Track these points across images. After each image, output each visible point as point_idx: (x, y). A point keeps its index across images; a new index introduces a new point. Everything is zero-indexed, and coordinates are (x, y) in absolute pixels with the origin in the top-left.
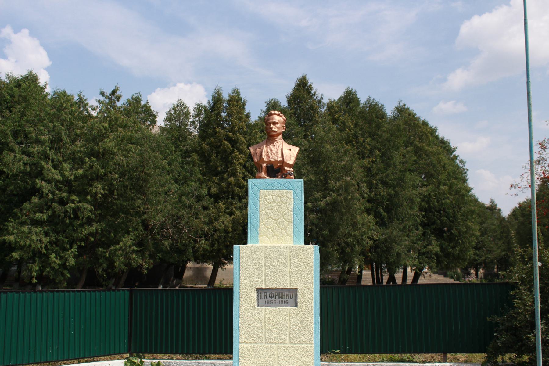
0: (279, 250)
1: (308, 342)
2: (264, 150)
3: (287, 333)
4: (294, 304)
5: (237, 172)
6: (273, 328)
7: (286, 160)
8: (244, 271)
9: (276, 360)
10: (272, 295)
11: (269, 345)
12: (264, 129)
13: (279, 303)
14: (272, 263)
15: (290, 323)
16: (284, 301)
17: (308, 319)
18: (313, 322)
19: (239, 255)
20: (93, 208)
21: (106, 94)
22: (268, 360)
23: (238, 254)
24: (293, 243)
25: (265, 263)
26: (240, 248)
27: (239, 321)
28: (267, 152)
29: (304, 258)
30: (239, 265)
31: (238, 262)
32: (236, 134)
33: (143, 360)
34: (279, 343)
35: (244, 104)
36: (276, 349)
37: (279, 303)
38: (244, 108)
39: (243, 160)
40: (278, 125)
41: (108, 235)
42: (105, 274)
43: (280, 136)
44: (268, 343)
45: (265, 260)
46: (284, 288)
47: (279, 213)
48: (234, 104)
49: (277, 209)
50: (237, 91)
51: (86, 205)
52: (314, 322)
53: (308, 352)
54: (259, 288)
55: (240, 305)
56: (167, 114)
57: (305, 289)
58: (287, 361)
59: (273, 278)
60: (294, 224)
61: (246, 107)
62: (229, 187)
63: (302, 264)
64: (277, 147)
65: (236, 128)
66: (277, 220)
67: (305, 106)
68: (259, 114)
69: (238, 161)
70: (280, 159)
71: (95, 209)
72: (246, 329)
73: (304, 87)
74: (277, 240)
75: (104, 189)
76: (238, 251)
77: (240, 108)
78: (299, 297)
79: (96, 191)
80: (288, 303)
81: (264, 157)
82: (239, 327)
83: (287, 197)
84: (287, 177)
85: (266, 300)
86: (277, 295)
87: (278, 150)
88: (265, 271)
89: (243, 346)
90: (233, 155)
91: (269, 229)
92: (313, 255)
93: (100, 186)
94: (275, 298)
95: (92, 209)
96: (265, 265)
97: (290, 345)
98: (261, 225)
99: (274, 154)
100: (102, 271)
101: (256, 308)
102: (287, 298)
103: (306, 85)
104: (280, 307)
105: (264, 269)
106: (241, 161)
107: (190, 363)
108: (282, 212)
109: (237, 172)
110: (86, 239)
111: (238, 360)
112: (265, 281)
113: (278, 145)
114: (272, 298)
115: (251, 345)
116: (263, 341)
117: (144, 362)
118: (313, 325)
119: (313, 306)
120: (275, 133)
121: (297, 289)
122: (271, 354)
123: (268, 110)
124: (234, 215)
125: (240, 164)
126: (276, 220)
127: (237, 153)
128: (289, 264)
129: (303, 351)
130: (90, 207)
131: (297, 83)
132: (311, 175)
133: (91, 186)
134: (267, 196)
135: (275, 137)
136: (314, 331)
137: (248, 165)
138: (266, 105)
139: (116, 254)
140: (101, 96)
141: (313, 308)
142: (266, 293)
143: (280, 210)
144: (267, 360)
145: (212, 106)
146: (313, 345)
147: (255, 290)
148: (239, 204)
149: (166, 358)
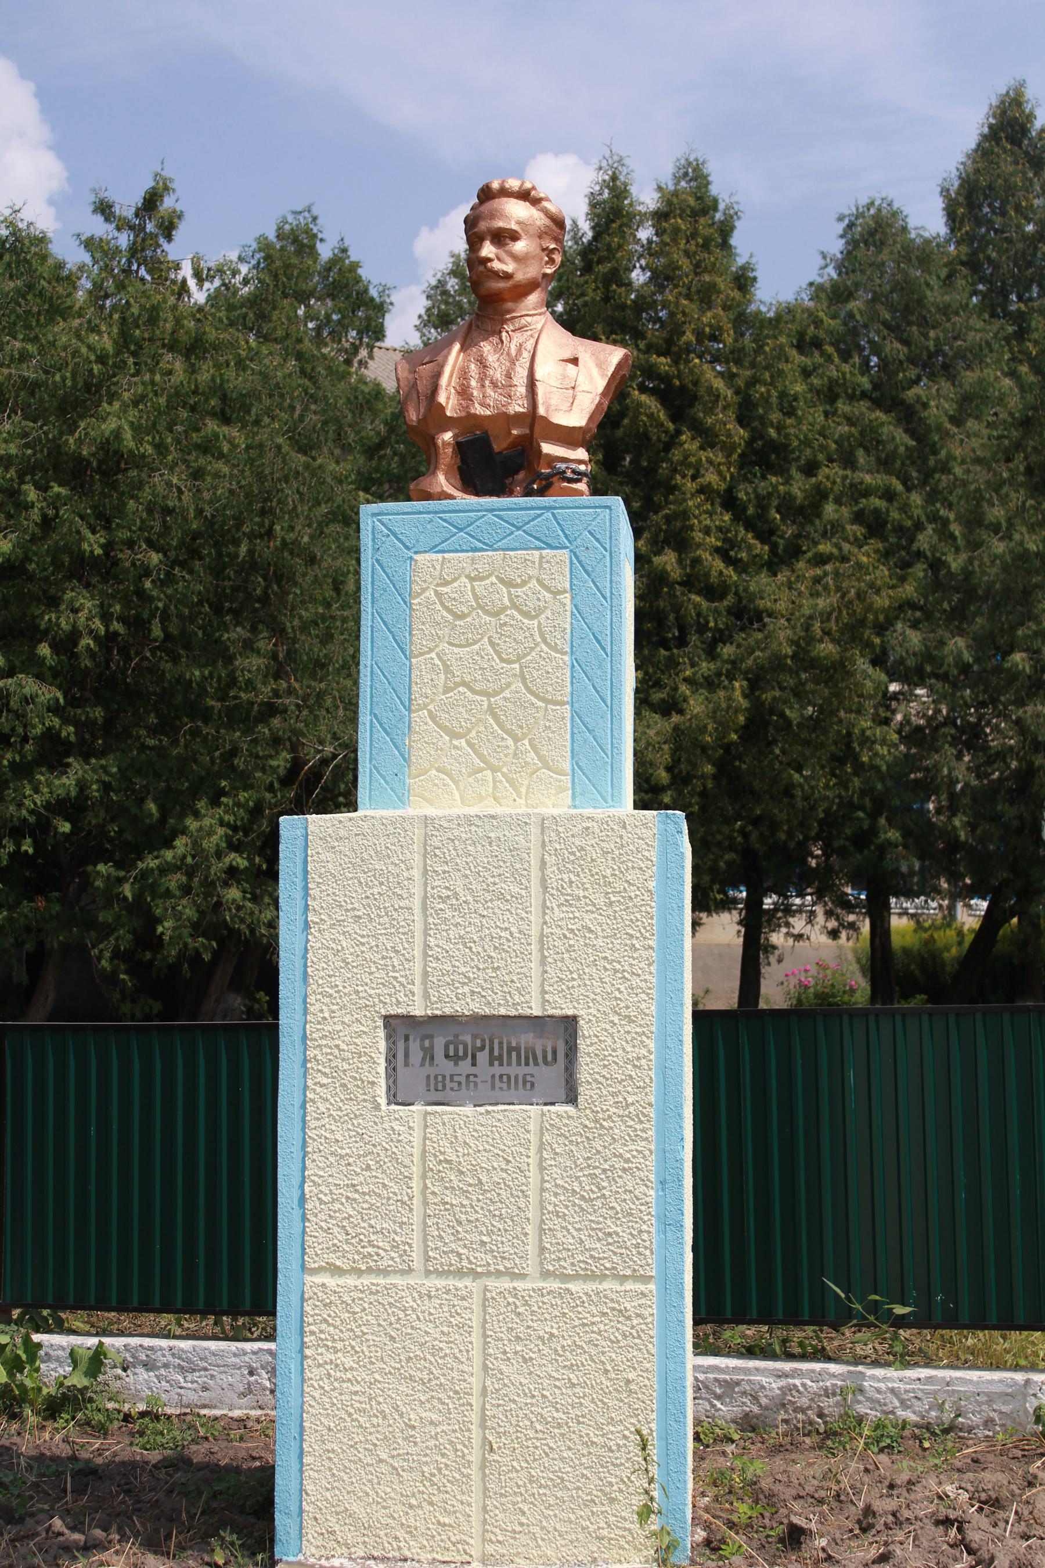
0: (492, 835)
1: (628, 1272)
2: (447, 370)
3: (529, 1229)
4: (562, 1094)
5: (691, 528)
6: (463, 1206)
7: (547, 411)
8: (327, 935)
9: (476, 1354)
10: (456, 1050)
11: (440, 1283)
12: (822, 334)
13: (493, 1087)
14: (456, 895)
15: (543, 1181)
16: (516, 1077)
17: (627, 1161)
18: (652, 1177)
19: (306, 862)
20: (59, 695)
21: (117, 210)
22: (435, 1351)
23: (299, 860)
24: (569, 802)
25: (425, 897)
26: (311, 828)
27: (304, 1168)
28: (464, 375)
29: (609, 872)
30: (307, 906)
31: (298, 895)
32: (688, 361)
33: (36, 1338)
34: (489, 1274)
35: (726, 230)
36: (476, 1301)
37: (493, 1087)
38: (725, 245)
39: (720, 473)
40: (520, 246)
41: (134, 810)
42: (127, 973)
43: (534, 298)
44: (436, 1271)
45: (426, 884)
46: (513, 1013)
47: (502, 660)
48: (676, 230)
49: (492, 644)
50: (697, 169)
51: (30, 685)
52: (657, 1174)
53: (629, 1318)
54: (397, 1016)
55: (310, 1095)
56: (428, 297)
57: (616, 1019)
58: (525, 1361)
59: (463, 969)
60: (575, 713)
61: (734, 241)
62: (658, 595)
63: (601, 901)
64: (513, 352)
65: (689, 336)
66: (496, 693)
67: (1019, 227)
68: (816, 271)
69: (694, 478)
70: (518, 407)
71: (73, 701)
72: (337, 1206)
73: (1016, 142)
74: (495, 788)
75: (106, 617)
76: (300, 842)
77: (706, 246)
78: (583, 1059)
79: (74, 625)
80: (532, 1085)
81: (448, 399)
82: (303, 1199)
83: (540, 582)
84: (551, 491)
85: (432, 1071)
86: (482, 1048)
87: (513, 362)
88: (426, 934)
89: (323, 1285)
90: (676, 455)
91: (459, 736)
92: (653, 855)
93: (88, 604)
94: (474, 1064)
95: (58, 700)
96: (424, 908)
97: (541, 1284)
98: (420, 718)
99: (494, 385)
100: (111, 959)
101: (384, 1107)
102: (527, 1064)
103: (1024, 131)
104: (497, 1104)
105: (418, 927)
106: (711, 477)
107: (235, 1355)
108: (519, 658)
109: (691, 528)
110: (40, 828)
111: (301, 1351)
112: (424, 983)
113: (518, 338)
114: (456, 1064)
115: (358, 1283)
116: (415, 1265)
117: (39, 1345)
118: (652, 1192)
119: (653, 1100)
120: (502, 285)
121: (574, 1019)
122: (450, 1325)
123: (849, 253)
124: (681, 712)
125: (704, 490)
126: (488, 695)
127: (692, 446)
128: (535, 902)
129: (604, 1314)
130: (48, 693)
131: (991, 126)
132: (1024, 529)
133: (53, 602)
134: (446, 583)
135: (504, 300)
136: (658, 1218)
137: (747, 494)
138: (840, 228)
139: (162, 890)
140: (100, 218)
141: (652, 1113)
142: (431, 1037)
143: (508, 648)
144: (433, 1355)
145: (590, 243)
146: (652, 1286)
147: (380, 1023)
148: (706, 667)
149: (179, 1331)
